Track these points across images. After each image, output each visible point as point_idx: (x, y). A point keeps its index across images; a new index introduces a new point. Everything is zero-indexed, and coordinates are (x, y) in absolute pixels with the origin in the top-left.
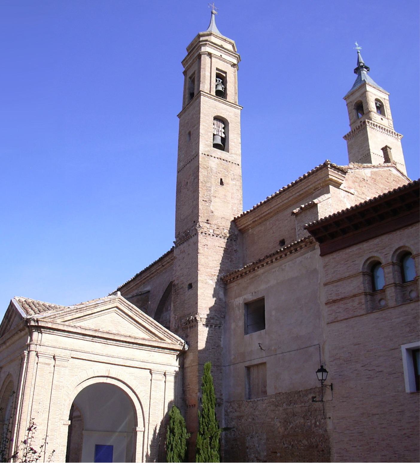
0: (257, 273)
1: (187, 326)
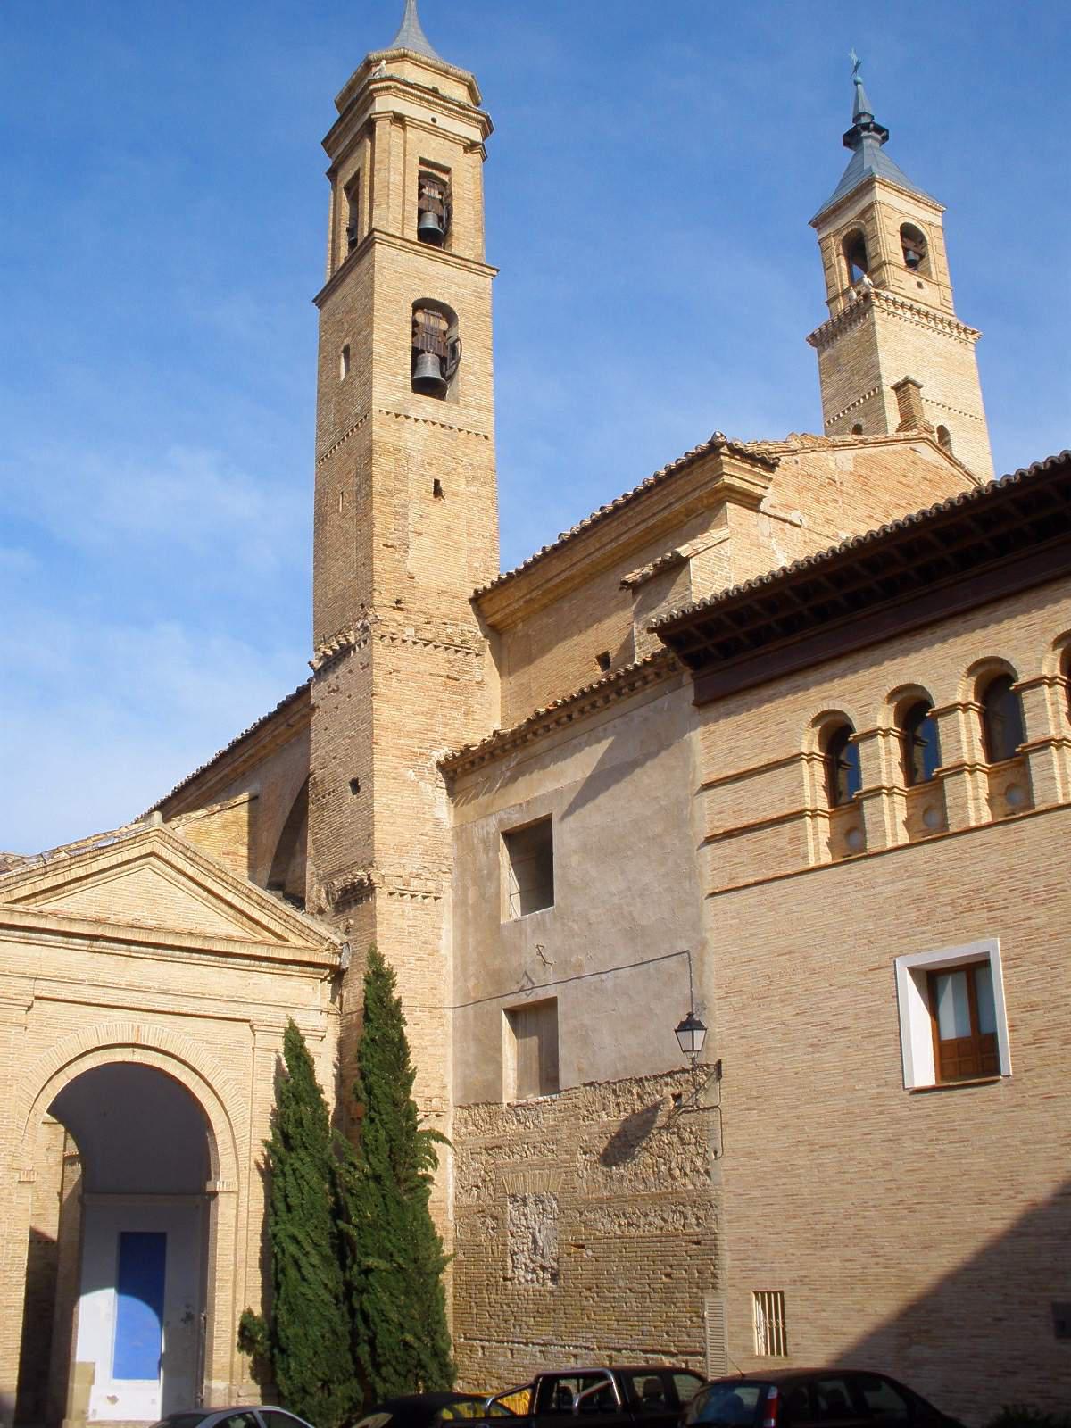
0: (533, 750)
1: (347, 897)
